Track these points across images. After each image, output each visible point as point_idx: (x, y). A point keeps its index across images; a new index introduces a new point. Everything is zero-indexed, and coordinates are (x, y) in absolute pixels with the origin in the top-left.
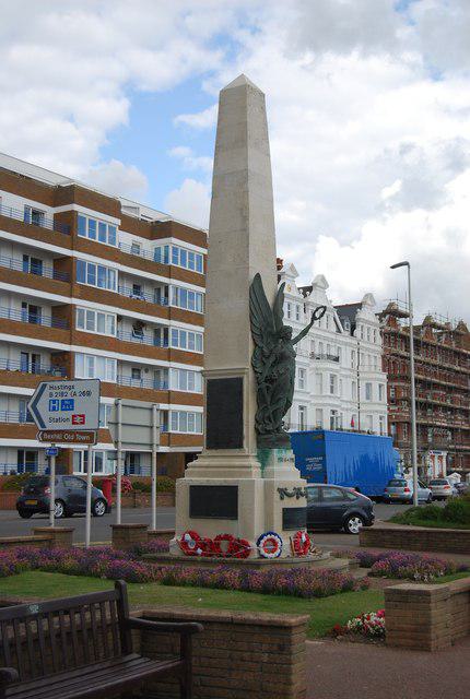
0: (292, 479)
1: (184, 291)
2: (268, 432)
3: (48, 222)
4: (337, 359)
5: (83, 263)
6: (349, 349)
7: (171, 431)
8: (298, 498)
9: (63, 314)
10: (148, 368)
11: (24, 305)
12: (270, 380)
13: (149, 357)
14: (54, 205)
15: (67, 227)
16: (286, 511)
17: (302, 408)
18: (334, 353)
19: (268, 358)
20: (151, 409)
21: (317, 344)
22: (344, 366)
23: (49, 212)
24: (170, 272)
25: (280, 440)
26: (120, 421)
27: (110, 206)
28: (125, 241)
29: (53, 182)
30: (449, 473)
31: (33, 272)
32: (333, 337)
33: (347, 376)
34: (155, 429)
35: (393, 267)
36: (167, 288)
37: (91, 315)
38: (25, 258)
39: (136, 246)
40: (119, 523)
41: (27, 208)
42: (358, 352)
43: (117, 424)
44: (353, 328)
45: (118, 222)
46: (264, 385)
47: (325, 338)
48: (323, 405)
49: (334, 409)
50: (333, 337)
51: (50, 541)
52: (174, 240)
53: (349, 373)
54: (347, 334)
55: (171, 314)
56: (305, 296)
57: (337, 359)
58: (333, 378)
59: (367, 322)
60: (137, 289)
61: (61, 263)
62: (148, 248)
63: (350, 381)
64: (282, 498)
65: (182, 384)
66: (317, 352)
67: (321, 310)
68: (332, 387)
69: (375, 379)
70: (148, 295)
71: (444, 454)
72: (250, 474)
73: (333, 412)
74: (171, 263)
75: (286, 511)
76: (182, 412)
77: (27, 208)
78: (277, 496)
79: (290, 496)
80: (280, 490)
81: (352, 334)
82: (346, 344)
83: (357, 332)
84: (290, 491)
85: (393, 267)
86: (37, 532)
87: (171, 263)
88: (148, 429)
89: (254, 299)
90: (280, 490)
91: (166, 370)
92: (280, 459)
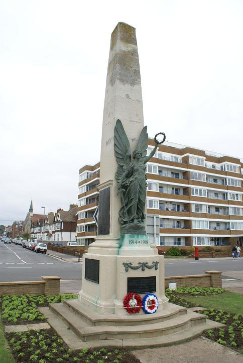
1: (232, 180)
3: (180, 161)
5: (193, 172)
7: (231, 229)
9: (186, 191)
10: (221, 207)
11: (173, 189)
13: (221, 203)
14: (181, 155)
15: (186, 161)
16: (130, 280)
20: (153, 217)
23: (180, 157)
24: (226, 173)
26: (155, 224)
27: (201, 153)
28: (209, 164)
29: (181, 147)
31: (176, 177)
34: (155, 226)
36: (226, 179)
37: (201, 191)
38: (172, 173)
39: (214, 167)
41: (171, 156)
45: (205, 158)
51: (210, 277)
52: (226, 162)
55: (228, 188)
60: (215, 181)
61: (185, 174)
62: (218, 166)
64: (127, 271)
70: (219, 183)
75: (130, 280)
76: (235, 223)
77: (171, 156)
80: (124, 264)
84: (150, 264)
86: (206, 273)
87: (226, 170)
89: (118, 138)
90: (124, 264)
91: (228, 207)
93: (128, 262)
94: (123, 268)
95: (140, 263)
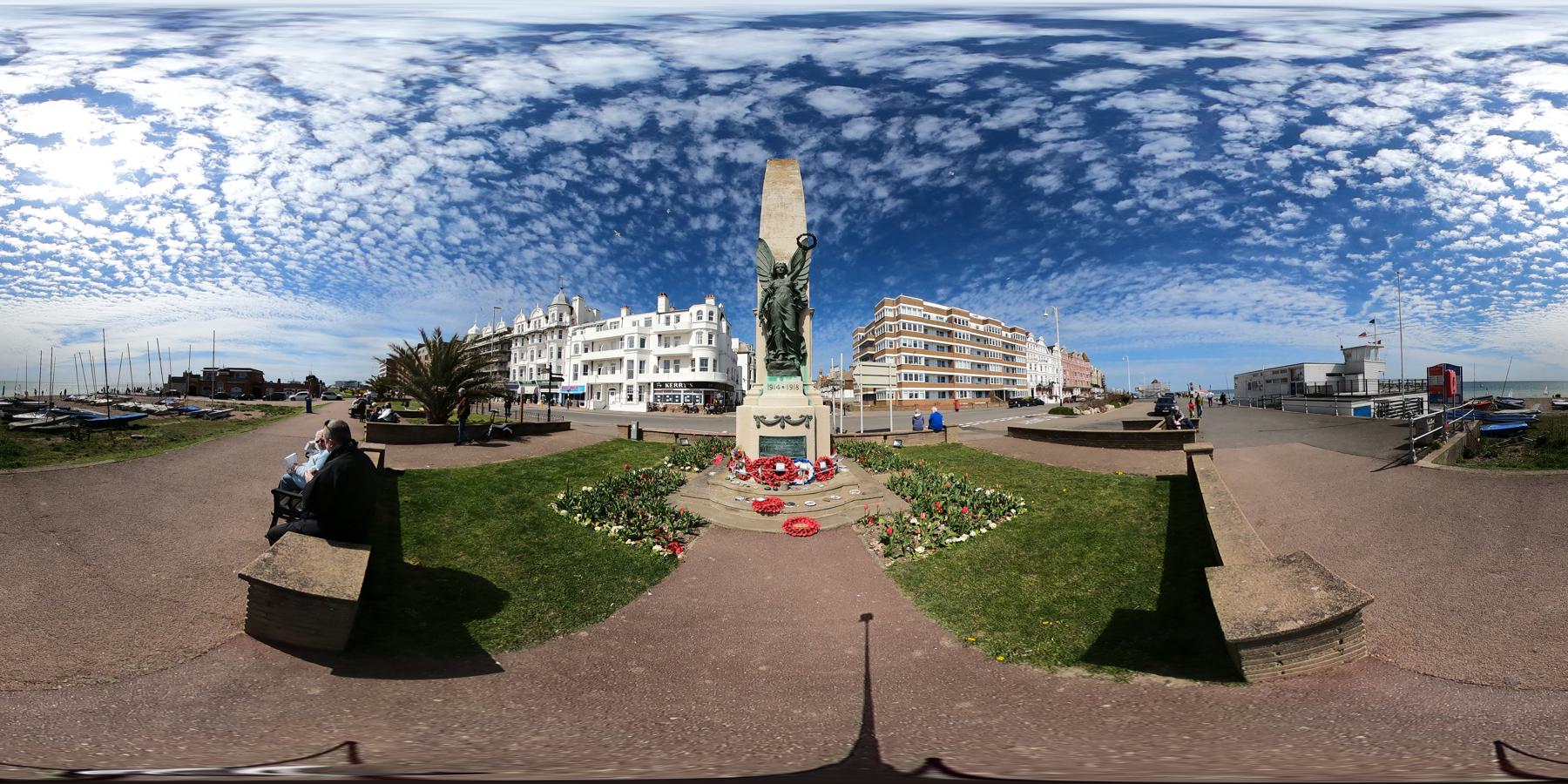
64: (759, 427)
80: (756, 418)
90: (756, 418)
94: (754, 423)
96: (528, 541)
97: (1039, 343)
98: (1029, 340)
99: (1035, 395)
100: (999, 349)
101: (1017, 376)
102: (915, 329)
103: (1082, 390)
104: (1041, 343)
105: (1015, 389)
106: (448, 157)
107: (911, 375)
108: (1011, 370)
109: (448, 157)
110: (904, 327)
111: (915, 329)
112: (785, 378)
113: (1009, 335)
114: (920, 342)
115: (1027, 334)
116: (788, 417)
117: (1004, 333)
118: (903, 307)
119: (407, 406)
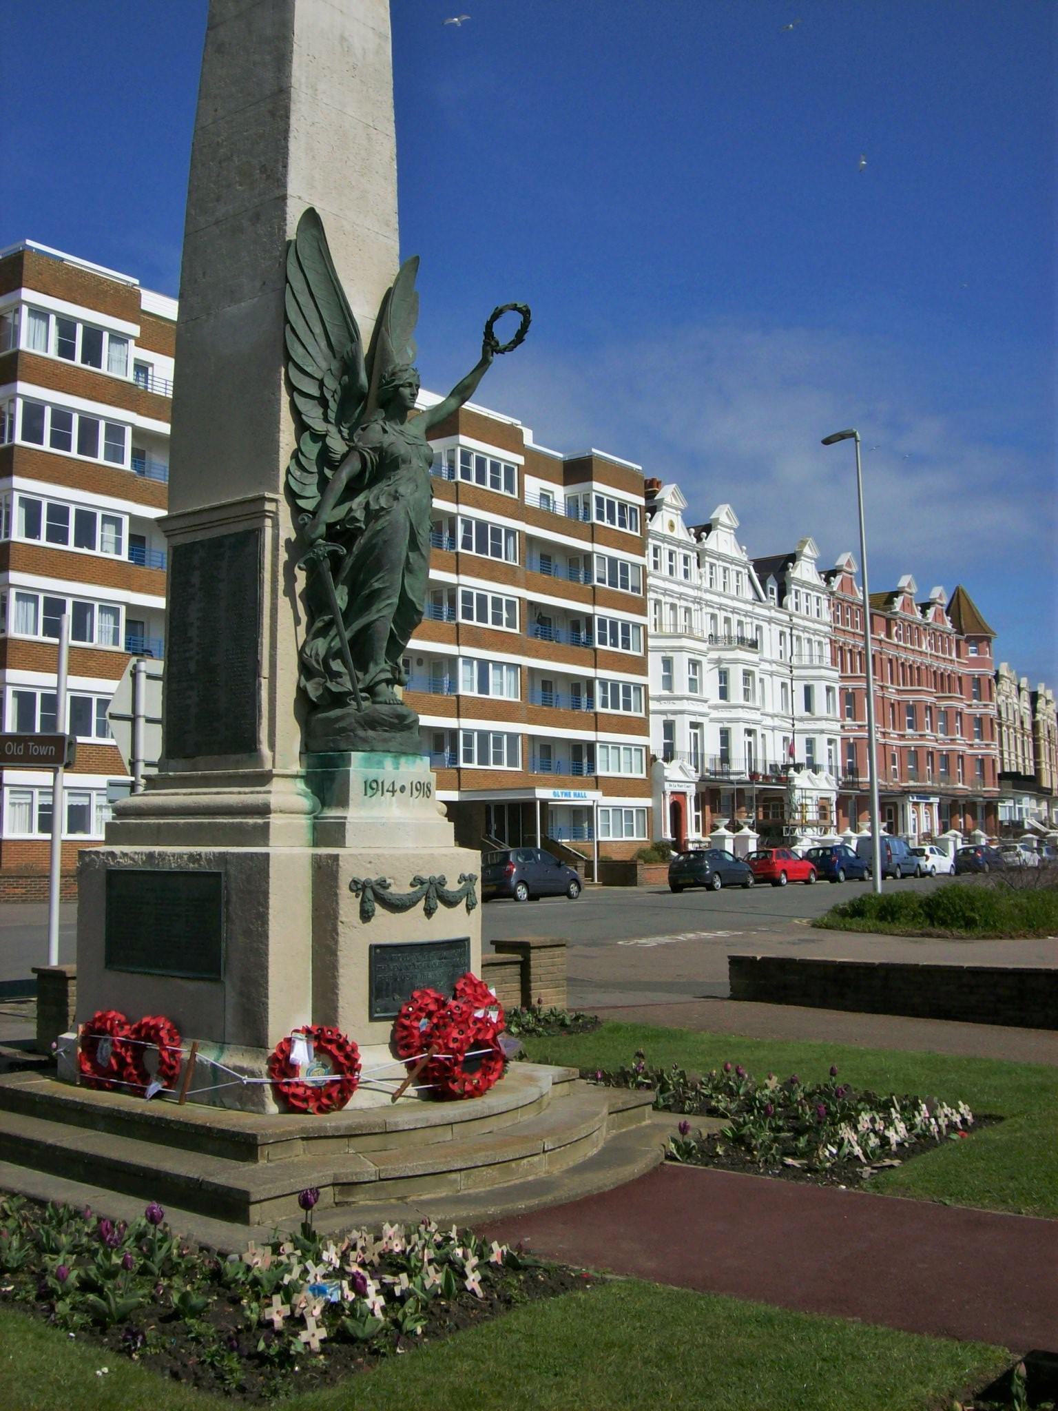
0: (408, 846)
2: (338, 700)
4: (754, 645)
6: (776, 629)
8: (429, 912)
12: (342, 533)
17: (694, 725)
18: (749, 634)
19: (335, 467)
21: (721, 620)
22: (767, 655)
25: (372, 723)
26: (142, 711)
30: (944, 829)
32: (749, 608)
33: (772, 674)
35: (827, 442)
40: (54, 962)
42: (790, 633)
43: (133, 720)
44: (782, 593)
46: (323, 547)
47: (734, 611)
48: (731, 720)
49: (753, 727)
50: (749, 608)
53: (775, 668)
54: (774, 603)
56: (699, 539)
57: (754, 645)
58: (747, 674)
59: (804, 584)
63: (778, 681)
64: (366, 915)
65: (483, 686)
66: (722, 630)
67: (515, 320)
68: (746, 691)
69: (820, 678)
71: (935, 800)
72: (262, 835)
73: (750, 732)
74: (459, 478)
75: (381, 955)
78: (349, 906)
79: (397, 906)
81: (780, 604)
82: (770, 621)
83: (790, 600)
84: (400, 888)
85: (827, 442)
88: (128, 724)
90: (358, 887)
92: (372, 787)
93: (374, 878)
95: (418, 881)
96: (772, 1129)
97: (712, 542)
98: (658, 524)
99: (692, 835)
100: (506, 575)
101: (597, 723)
102: (87, 445)
103: (952, 809)
104: (722, 541)
105: (591, 797)
106: (170, 1248)
107: (58, 513)
108: (562, 691)
109: (170, 1248)
110: (32, 432)
111: (87, 445)
112: (403, 760)
113: (559, 493)
114: (115, 431)
115: (650, 490)
116: (383, 884)
117: (533, 486)
118: (40, 313)
119: (150, 1210)
